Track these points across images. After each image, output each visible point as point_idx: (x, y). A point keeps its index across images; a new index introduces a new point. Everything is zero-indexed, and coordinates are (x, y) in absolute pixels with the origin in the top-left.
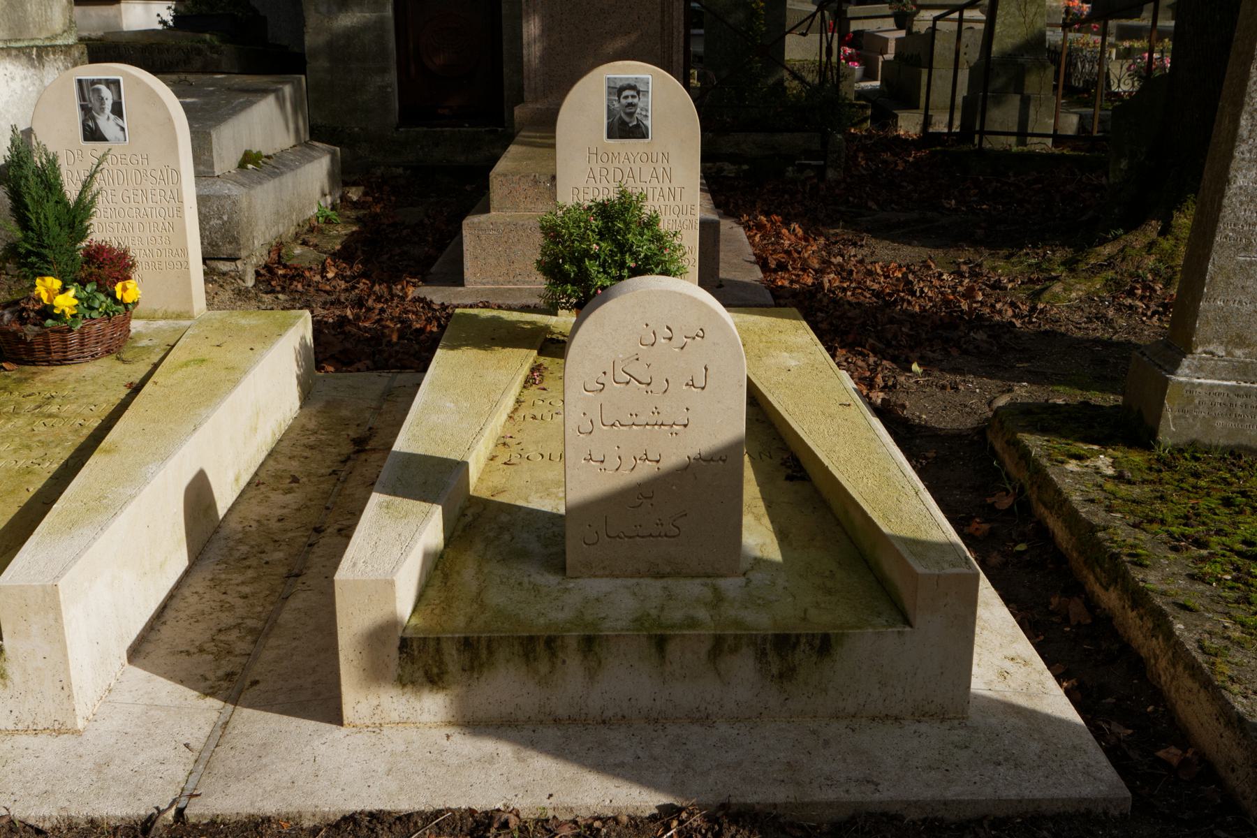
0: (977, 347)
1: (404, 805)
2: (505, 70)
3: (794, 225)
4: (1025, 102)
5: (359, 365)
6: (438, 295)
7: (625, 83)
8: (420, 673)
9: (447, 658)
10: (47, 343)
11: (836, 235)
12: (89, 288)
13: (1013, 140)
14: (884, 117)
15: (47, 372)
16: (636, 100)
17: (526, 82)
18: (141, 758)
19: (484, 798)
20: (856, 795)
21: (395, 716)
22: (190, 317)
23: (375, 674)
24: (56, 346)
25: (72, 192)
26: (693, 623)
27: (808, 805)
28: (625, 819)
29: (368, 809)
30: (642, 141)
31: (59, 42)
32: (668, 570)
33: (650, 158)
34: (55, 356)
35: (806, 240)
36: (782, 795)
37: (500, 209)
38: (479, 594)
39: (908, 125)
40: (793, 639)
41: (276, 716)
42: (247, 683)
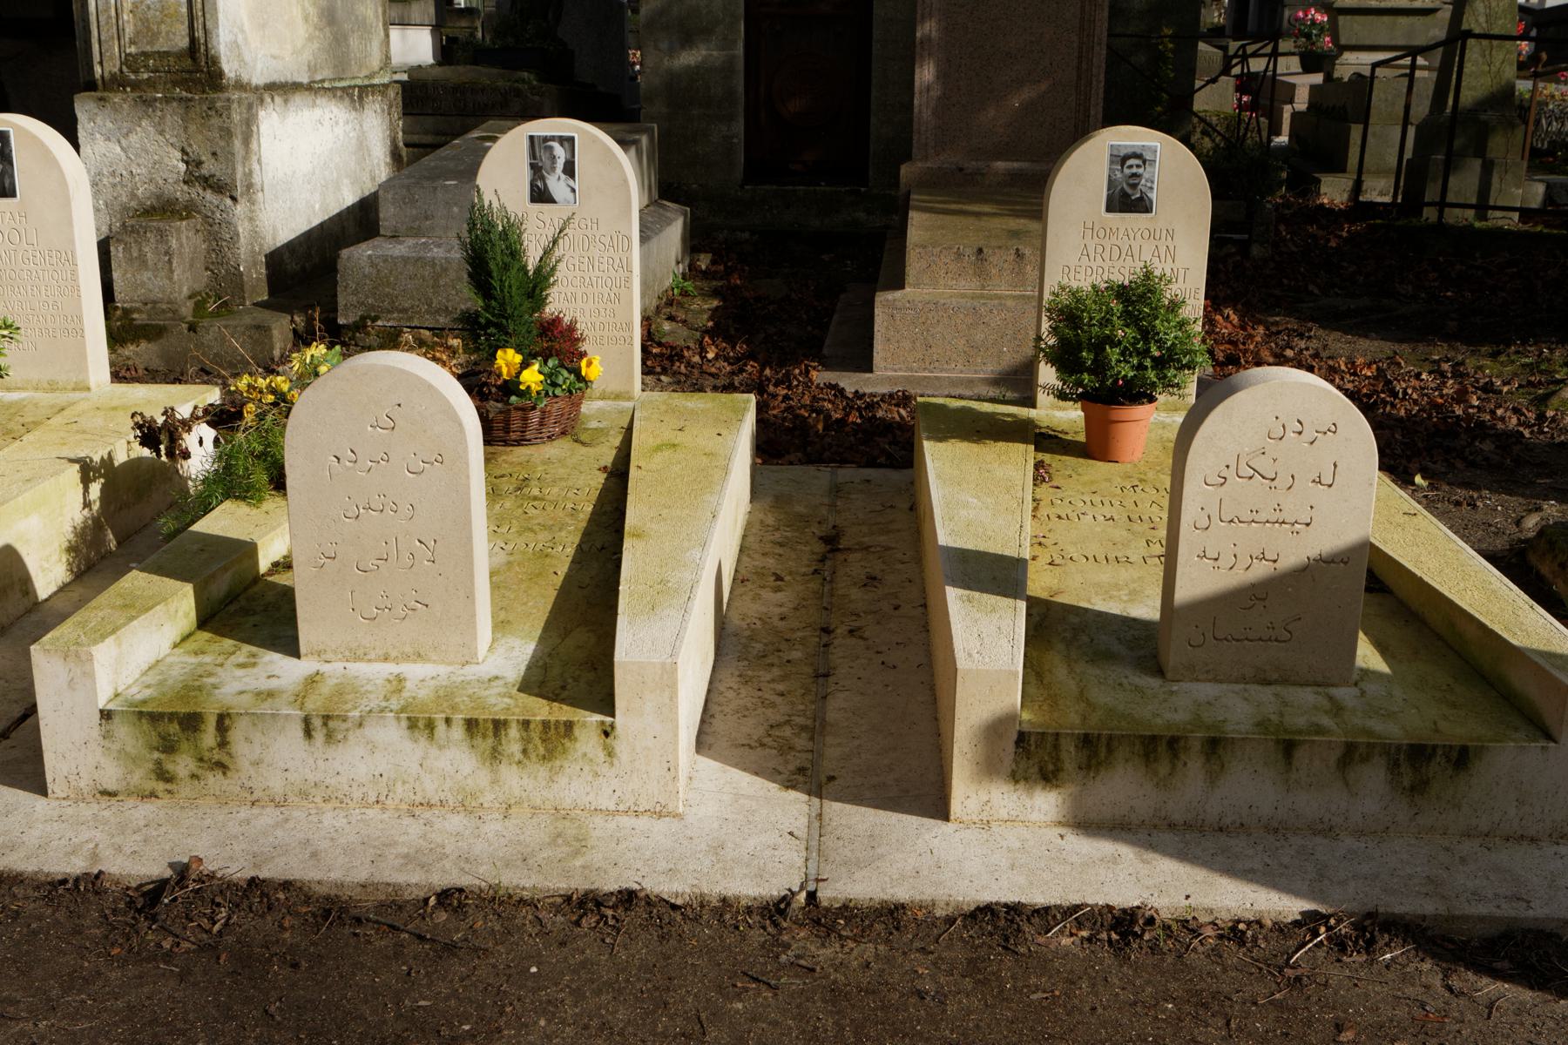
0: (1486, 459)
1: (1039, 898)
2: (873, 120)
3: (1229, 311)
4: (1488, 168)
5: (792, 457)
6: (850, 382)
7: (1130, 151)
8: (1035, 769)
9: (1064, 755)
10: (507, 422)
11: (1276, 324)
12: (551, 363)
13: (1470, 213)
14: (1305, 184)
15: (506, 453)
16: (1141, 171)
17: (915, 138)
18: (751, 843)
19: (1124, 895)
20: (1508, 910)
21: (1003, 814)
22: (630, 399)
23: (989, 768)
24: (516, 425)
25: (532, 259)
26: (1319, 730)
27: (1458, 918)
28: (1269, 923)
29: (1003, 900)
30: (1144, 215)
31: (376, 81)
32: (1275, 676)
33: (1152, 235)
34: (513, 436)
35: (1243, 328)
36: (1429, 907)
37: (916, 285)
38: (1082, 692)
39: (1333, 191)
40: (1429, 751)
41: (871, 811)
42: (824, 780)
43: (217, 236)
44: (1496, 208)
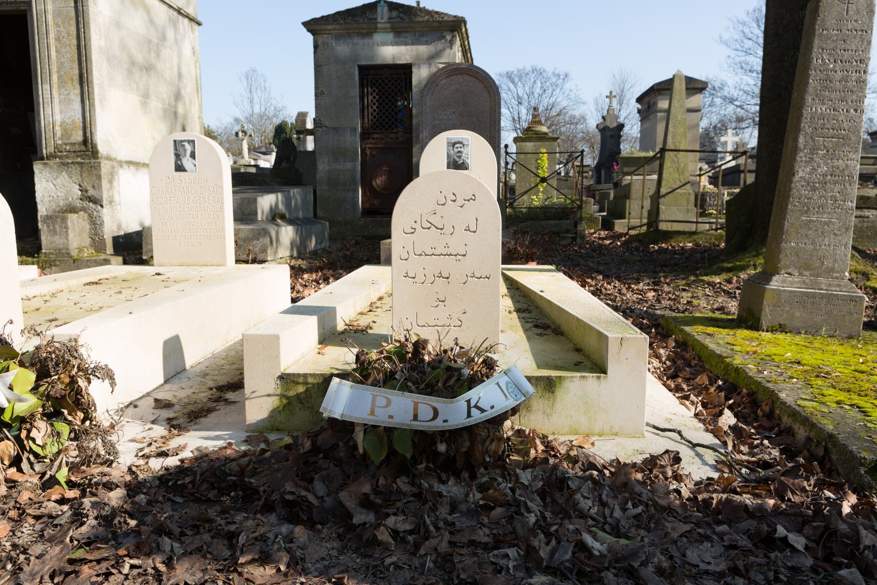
7: (456, 140)
43: (95, 224)
44: (662, 221)
